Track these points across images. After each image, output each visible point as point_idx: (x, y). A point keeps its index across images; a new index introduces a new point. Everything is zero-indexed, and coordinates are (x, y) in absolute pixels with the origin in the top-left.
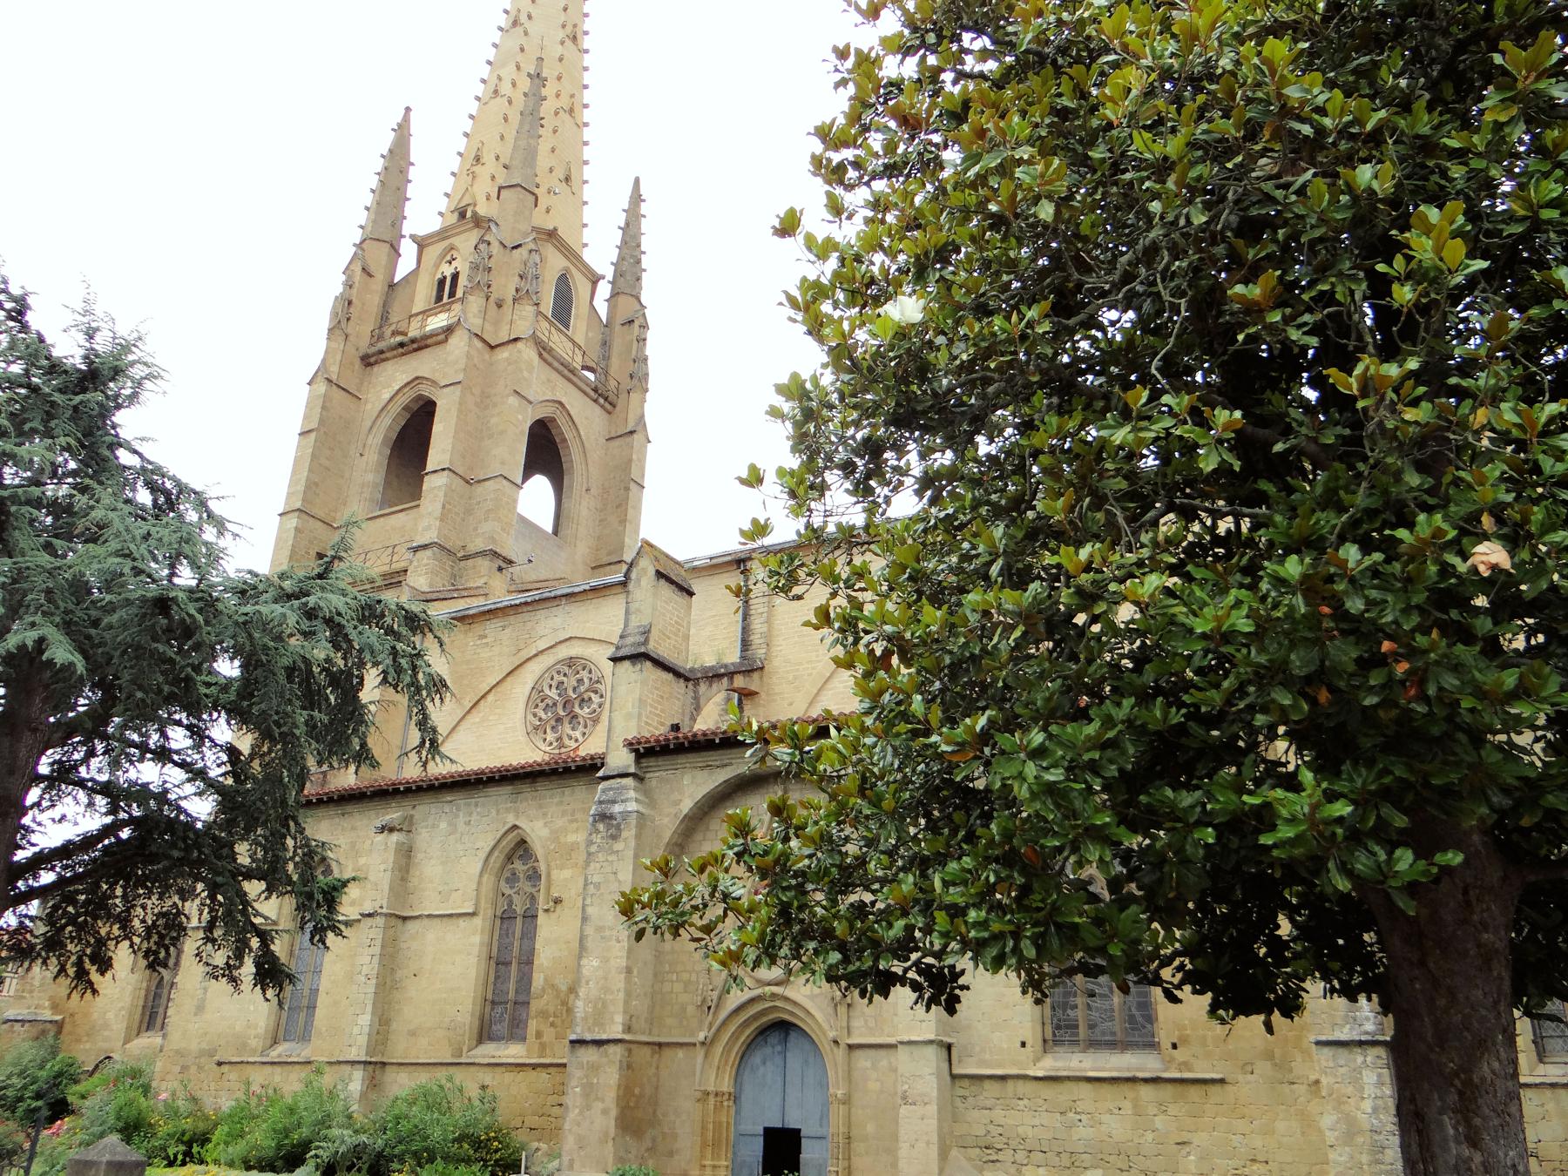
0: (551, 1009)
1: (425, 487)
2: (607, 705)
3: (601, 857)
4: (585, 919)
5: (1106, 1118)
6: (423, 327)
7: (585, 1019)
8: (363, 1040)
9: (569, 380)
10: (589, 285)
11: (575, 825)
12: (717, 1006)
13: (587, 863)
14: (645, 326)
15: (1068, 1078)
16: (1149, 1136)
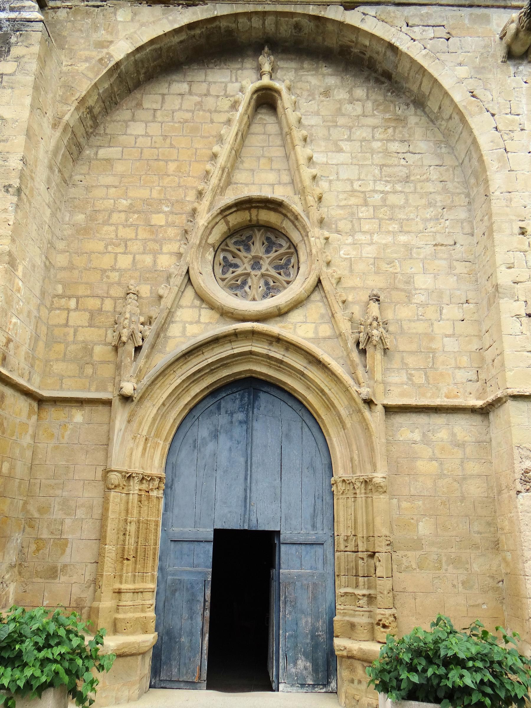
12: (153, 346)
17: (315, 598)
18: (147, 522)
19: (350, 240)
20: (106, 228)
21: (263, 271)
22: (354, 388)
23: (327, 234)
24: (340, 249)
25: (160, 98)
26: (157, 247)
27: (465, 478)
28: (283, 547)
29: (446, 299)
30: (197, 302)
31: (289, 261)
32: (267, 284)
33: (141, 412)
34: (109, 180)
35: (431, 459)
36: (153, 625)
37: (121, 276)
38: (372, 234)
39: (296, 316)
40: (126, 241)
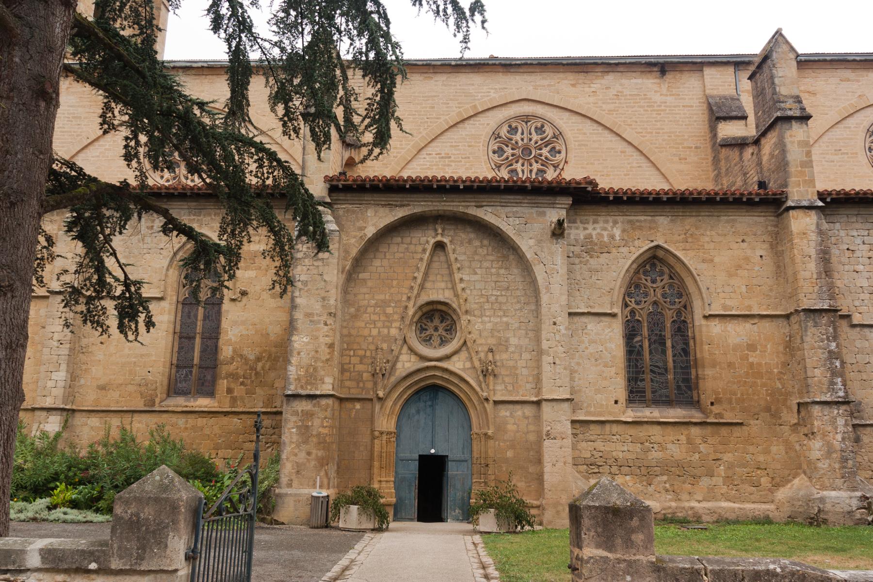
0: (241, 372)
5: (669, 446)
7: (298, 379)
8: (59, 392)
12: (390, 374)
15: (647, 423)
16: (697, 456)
17: (463, 484)
18: (390, 452)
19: (480, 320)
20: (365, 315)
21: (439, 333)
22: (480, 393)
23: (469, 318)
24: (475, 324)
25: (387, 245)
26: (389, 324)
27: (528, 432)
28: (450, 463)
29: (524, 350)
30: (409, 352)
31: (452, 327)
32: (441, 339)
33: (386, 404)
34: (364, 290)
35: (514, 424)
36: (394, 495)
37: (373, 339)
38: (490, 317)
39: (455, 358)
40: (374, 322)
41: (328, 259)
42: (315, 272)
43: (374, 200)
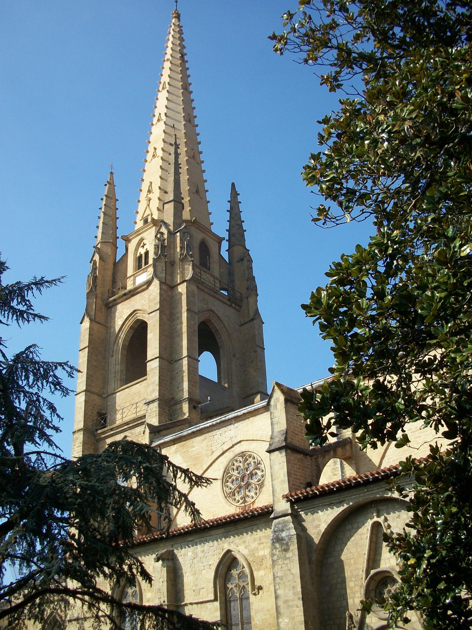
1: (148, 369)
2: (255, 456)
3: (280, 562)
4: (277, 597)
6: (134, 283)
9: (215, 297)
10: (217, 245)
11: (262, 546)
13: (273, 566)
14: (250, 261)
41: (292, 557)
42: (286, 568)
43: (321, 503)
